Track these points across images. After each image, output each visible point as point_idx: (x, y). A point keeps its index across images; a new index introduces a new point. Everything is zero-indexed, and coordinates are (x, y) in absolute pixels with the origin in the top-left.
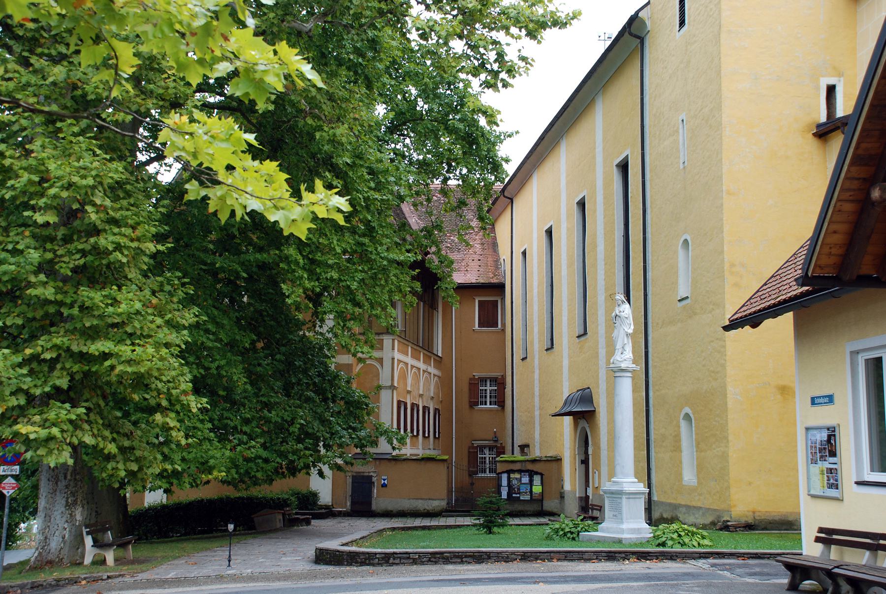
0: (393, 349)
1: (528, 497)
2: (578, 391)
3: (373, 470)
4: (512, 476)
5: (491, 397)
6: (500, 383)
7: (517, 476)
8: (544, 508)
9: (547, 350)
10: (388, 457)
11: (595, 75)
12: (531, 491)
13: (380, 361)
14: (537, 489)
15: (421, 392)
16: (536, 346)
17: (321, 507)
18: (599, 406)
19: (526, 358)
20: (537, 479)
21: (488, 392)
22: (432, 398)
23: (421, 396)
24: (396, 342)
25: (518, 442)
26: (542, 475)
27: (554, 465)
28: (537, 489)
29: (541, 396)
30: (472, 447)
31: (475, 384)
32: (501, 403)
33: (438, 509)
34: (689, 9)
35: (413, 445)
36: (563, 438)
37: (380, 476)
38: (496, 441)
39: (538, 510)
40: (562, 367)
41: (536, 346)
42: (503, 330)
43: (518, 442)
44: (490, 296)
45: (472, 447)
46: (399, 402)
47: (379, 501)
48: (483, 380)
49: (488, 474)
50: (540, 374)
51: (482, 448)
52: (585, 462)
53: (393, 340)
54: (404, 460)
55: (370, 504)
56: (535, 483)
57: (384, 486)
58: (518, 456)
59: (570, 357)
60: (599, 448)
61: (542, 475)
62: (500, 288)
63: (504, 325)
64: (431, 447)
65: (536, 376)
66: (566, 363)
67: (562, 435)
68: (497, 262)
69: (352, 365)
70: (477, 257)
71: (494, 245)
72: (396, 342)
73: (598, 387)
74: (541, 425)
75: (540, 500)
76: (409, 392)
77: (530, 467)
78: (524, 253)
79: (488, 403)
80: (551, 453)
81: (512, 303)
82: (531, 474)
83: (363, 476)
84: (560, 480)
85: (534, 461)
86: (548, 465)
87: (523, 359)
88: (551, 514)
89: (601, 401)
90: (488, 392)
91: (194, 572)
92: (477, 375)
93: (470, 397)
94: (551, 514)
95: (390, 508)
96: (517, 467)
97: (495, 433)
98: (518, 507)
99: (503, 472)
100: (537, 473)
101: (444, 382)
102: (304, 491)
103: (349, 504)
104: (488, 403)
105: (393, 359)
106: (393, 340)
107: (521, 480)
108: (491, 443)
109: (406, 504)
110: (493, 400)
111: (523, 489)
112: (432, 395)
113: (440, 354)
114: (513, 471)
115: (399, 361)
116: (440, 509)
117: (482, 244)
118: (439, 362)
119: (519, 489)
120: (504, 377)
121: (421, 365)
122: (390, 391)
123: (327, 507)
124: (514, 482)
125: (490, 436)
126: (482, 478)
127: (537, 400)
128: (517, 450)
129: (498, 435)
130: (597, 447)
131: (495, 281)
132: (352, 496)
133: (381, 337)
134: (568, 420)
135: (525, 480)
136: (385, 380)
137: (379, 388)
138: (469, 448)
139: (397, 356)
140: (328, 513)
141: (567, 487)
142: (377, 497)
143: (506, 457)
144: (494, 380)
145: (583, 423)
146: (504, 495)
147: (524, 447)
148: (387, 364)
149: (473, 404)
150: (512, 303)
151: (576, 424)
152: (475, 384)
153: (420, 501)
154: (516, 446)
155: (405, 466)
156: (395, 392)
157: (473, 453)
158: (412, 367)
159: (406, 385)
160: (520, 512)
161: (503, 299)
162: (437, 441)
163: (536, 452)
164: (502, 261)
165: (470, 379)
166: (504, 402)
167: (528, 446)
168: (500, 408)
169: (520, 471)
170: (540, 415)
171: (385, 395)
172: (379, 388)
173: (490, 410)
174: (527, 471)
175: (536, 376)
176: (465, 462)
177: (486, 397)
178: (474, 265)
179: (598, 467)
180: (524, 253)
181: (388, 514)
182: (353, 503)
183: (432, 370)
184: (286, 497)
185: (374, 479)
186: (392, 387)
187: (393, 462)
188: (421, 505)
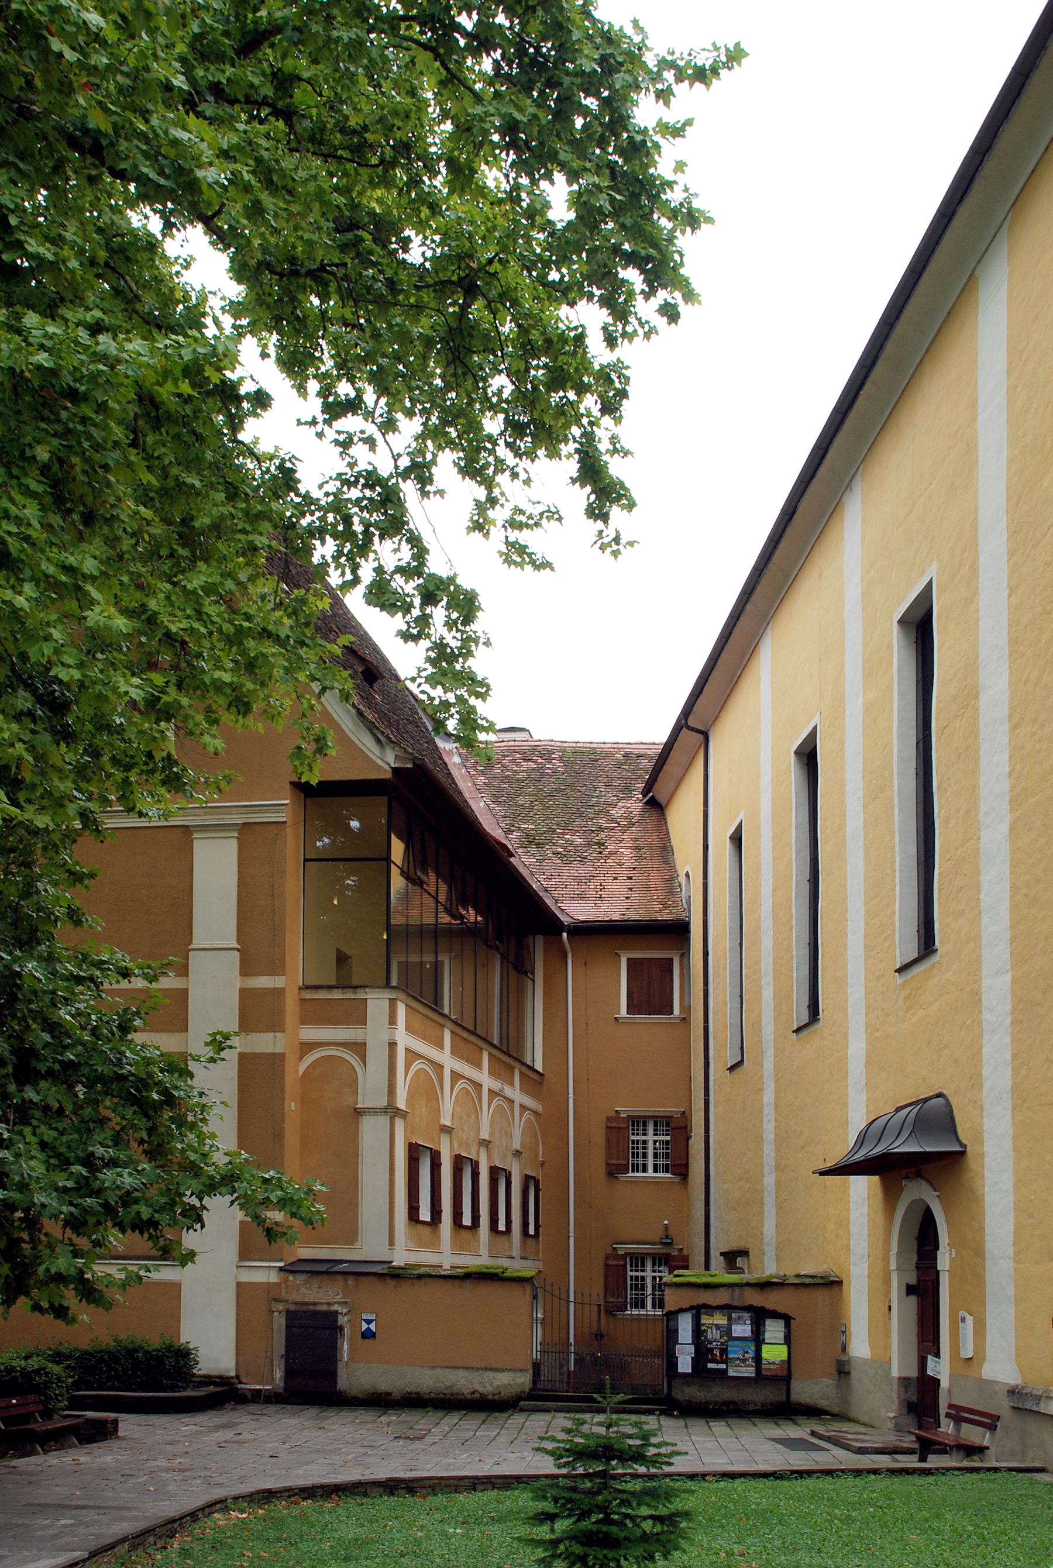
0: (393, 1021)
1: (749, 1371)
2: (898, 1109)
3: (339, 1298)
4: (705, 1320)
5: (656, 1156)
6: (677, 1128)
7: (720, 1320)
8: (794, 1397)
9: (797, 1031)
10: (378, 1269)
11: (990, 165)
12: (758, 1358)
13: (360, 1049)
14: (774, 1353)
15: (485, 1135)
16: (768, 1029)
17: (208, 1380)
18: (979, 1138)
19: (741, 1063)
20: (774, 1330)
21: (650, 1145)
22: (517, 1153)
23: (485, 1143)
24: (401, 1010)
25: (719, 1244)
26: (787, 1319)
27: (821, 1297)
28: (774, 1353)
29: (779, 1140)
30: (614, 1254)
31: (619, 1132)
32: (681, 1169)
33: (505, 1393)
34: (941, 782)
35: (458, 1246)
36: (855, 1232)
37: (356, 1311)
38: (669, 1245)
39: (774, 1401)
40: (844, 1060)
41: (768, 1029)
42: (685, 1020)
43: (719, 1244)
44: (655, 945)
45: (614, 1254)
46: (414, 1152)
47: (356, 1371)
48: (639, 1122)
49: (649, 1310)
50: (777, 1092)
51: (639, 1260)
52: (924, 1291)
53: (393, 1002)
54: (420, 1277)
55: (333, 1375)
56: (768, 1336)
57: (368, 1335)
58: (719, 1273)
59: (871, 1028)
60: (979, 1252)
61: (787, 1319)
62: (677, 932)
63: (686, 1009)
64: (516, 1252)
65: (768, 1097)
66: (857, 1049)
67: (844, 1224)
68: (670, 883)
69: (282, 1056)
70: (624, 873)
71: (665, 850)
72: (401, 1010)
73: (976, 1082)
74: (779, 1207)
75: (784, 1377)
76: (446, 1130)
77: (756, 1299)
78: (737, 839)
79: (650, 1168)
80: (808, 1268)
81: (706, 954)
82: (760, 1316)
83: (315, 1313)
84: (840, 1332)
85: (765, 1285)
86: (804, 1295)
87: (732, 1069)
88: (813, 1412)
89: (988, 1124)
90: (650, 1145)
91: (894, 1249)
92: (625, 1110)
93: (609, 1155)
94: (813, 1412)
95: (383, 1386)
96: (721, 1297)
97: (666, 1227)
98: (719, 1393)
99: (682, 1310)
100: (775, 1315)
101: (549, 1124)
102: (155, 1342)
103: (279, 1374)
104: (650, 1168)
105: (393, 1045)
106: (393, 1002)
107: (729, 1330)
108: (658, 1248)
109: (427, 1379)
110: (661, 1162)
111: (735, 1351)
112: (517, 1145)
113: (539, 1067)
114: (710, 1309)
115: (412, 1055)
116: (514, 1391)
117: (638, 848)
118: (534, 1081)
119: (724, 1351)
120: (686, 1117)
121: (487, 1081)
122: (385, 1120)
123: (222, 1381)
124: (712, 1334)
125: (658, 1234)
126: (638, 1319)
127: (769, 1151)
128: (717, 1262)
129: (672, 1232)
130: (974, 1251)
131: (666, 916)
132: (287, 1356)
133: (361, 994)
134: (862, 1189)
135: (742, 1329)
136: (370, 1090)
137: (358, 1113)
138: (607, 1257)
139: (404, 1039)
140: (224, 1395)
141: (860, 1348)
142: (351, 1358)
143: (688, 1275)
144: (663, 1122)
145: (918, 1191)
146: (685, 1365)
147: (731, 1257)
148: (377, 1056)
149: (614, 1171)
150: (706, 954)
151: (891, 1194)
152: (619, 1132)
153: (461, 1373)
154: (714, 1254)
155: (423, 1292)
156: (400, 1125)
157: (616, 1274)
158: (456, 1076)
159: (437, 1112)
160: (727, 1403)
161: (685, 955)
162: (531, 1242)
163: (768, 1268)
164: (682, 879)
165: (609, 1119)
166: (686, 1165)
167: (744, 1253)
168: (677, 1179)
169: (727, 1308)
170: (778, 1182)
171: (372, 1132)
172: (358, 1113)
173: (657, 1183)
174: (749, 1308)
175: (768, 1097)
176: (598, 1286)
177: (645, 1155)
178: (619, 888)
179: (974, 1300)
180: (737, 839)
181: (380, 1402)
182: (289, 1374)
183: (515, 1092)
184: (34, 1363)
185: (342, 1320)
186: (392, 1111)
187: (392, 1283)
188: (465, 1382)
